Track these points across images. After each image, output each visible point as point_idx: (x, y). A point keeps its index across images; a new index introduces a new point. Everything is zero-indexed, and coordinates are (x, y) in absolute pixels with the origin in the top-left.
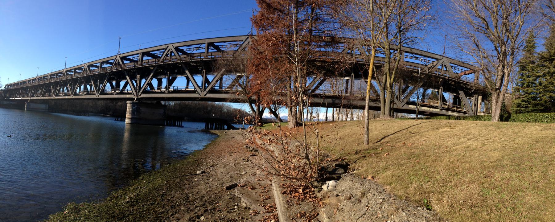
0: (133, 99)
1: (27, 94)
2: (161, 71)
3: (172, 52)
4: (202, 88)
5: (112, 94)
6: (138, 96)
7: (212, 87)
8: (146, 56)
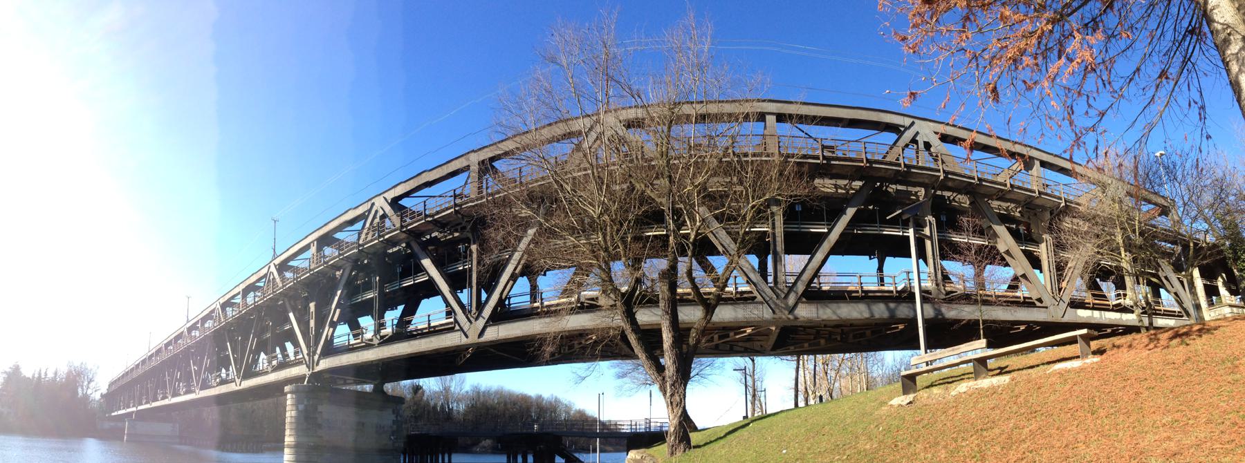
0: (300, 379)
2: (935, 192)
3: (384, 216)
4: (470, 312)
6: (313, 370)
7: (501, 302)
8: (326, 247)
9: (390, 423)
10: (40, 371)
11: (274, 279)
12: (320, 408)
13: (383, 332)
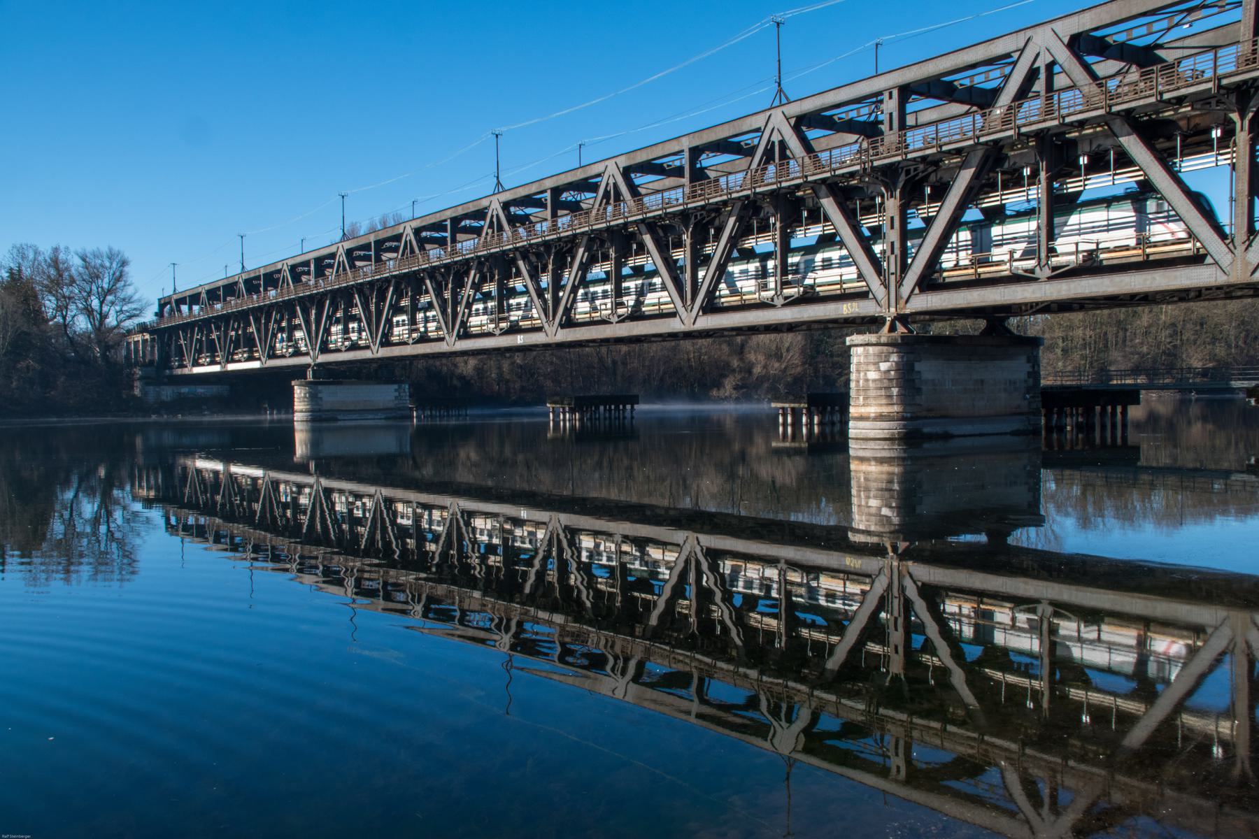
1: (212, 349)
5: (489, 335)
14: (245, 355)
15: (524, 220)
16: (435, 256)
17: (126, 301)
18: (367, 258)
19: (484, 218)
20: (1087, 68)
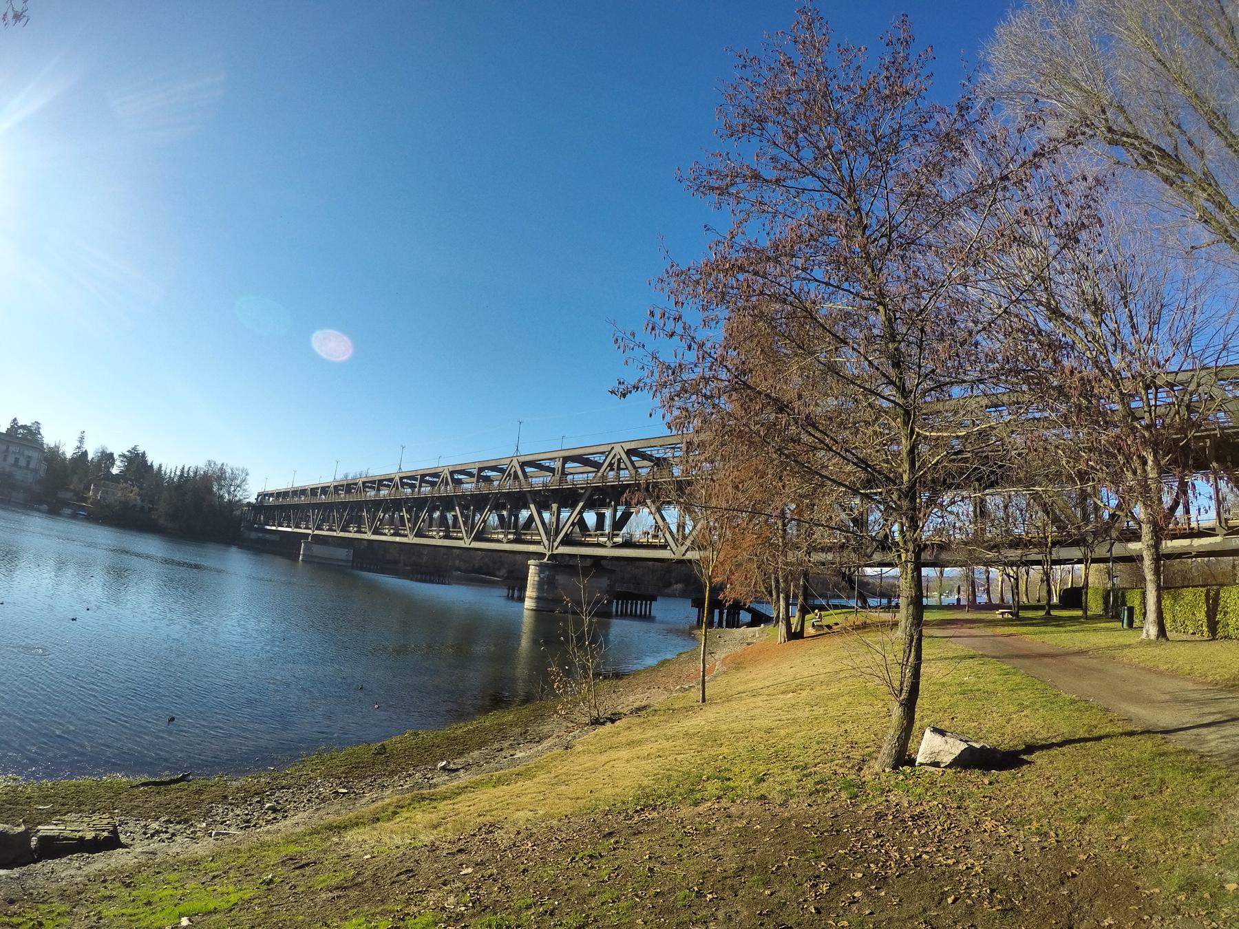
9: (606, 585)
10: (183, 468)
11: (515, 472)
12: (557, 577)
13: (616, 540)
14: (392, 531)
15: (459, 482)
16: (371, 494)
17: (245, 490)
18: (374, 488)
19: (439, 478)
20: (632, 462)
